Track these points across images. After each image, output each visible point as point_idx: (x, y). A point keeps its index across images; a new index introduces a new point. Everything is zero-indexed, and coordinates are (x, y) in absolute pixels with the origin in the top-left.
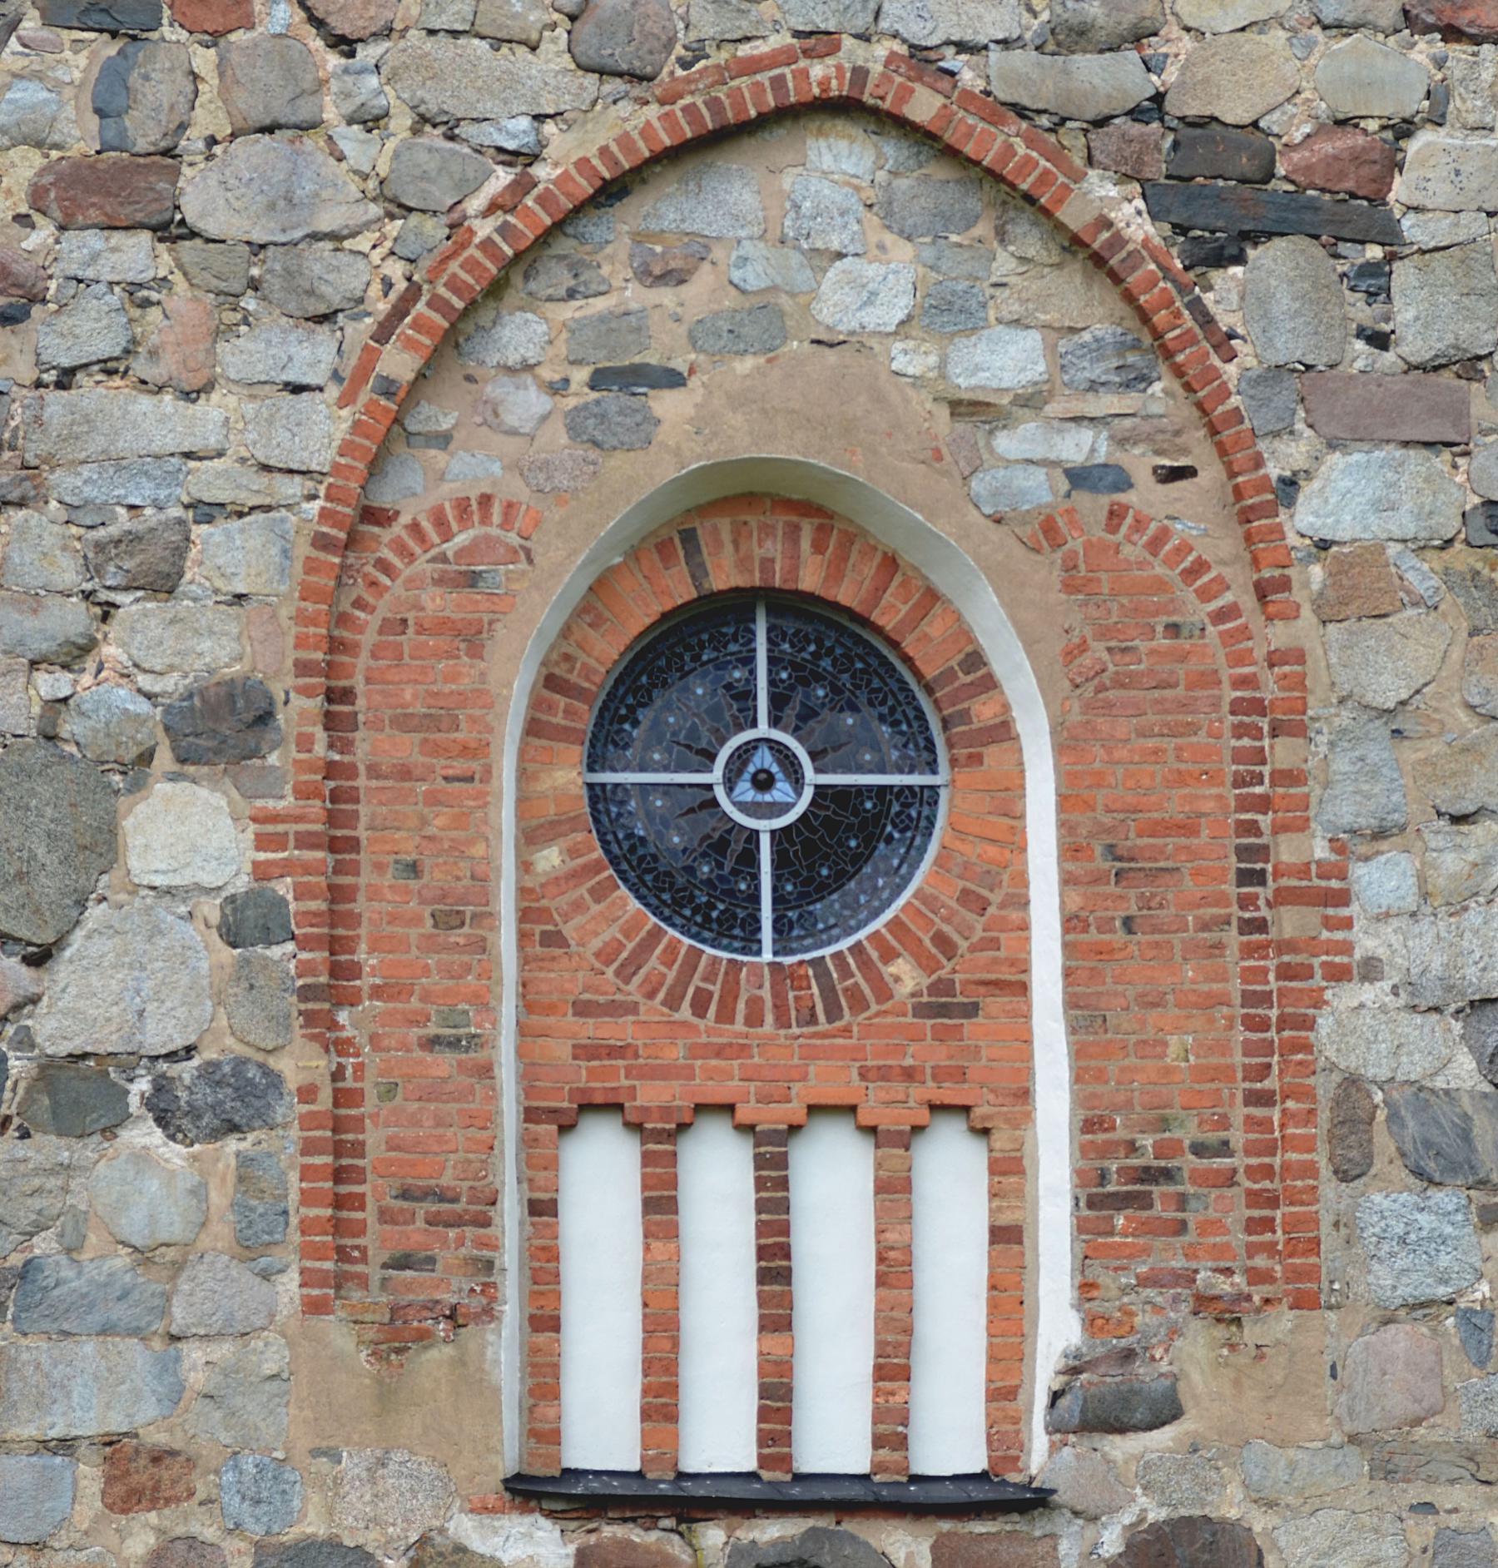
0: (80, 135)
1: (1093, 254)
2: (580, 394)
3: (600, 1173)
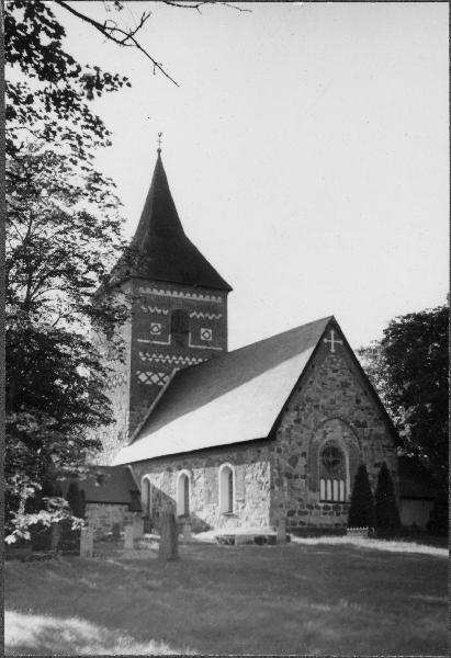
3: (323, 482)
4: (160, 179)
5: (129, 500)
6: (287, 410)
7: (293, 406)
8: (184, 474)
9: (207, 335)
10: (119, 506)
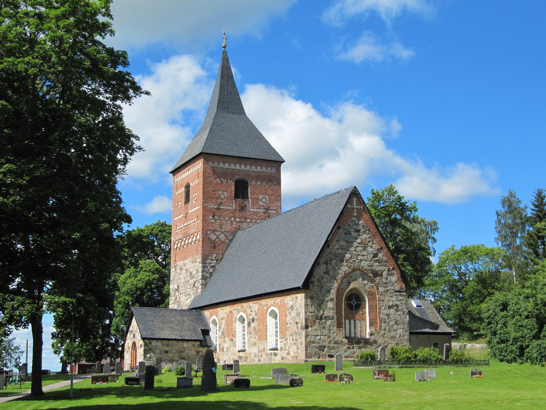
0: (325, 270)
1: (370, 277)
3: (347, 321)
4: (225, 53)
5: (201, 337)
6: (318, 264)
7: (322, 261)
8: (241, 316)
9: (264, 200)
10: (193, 342)
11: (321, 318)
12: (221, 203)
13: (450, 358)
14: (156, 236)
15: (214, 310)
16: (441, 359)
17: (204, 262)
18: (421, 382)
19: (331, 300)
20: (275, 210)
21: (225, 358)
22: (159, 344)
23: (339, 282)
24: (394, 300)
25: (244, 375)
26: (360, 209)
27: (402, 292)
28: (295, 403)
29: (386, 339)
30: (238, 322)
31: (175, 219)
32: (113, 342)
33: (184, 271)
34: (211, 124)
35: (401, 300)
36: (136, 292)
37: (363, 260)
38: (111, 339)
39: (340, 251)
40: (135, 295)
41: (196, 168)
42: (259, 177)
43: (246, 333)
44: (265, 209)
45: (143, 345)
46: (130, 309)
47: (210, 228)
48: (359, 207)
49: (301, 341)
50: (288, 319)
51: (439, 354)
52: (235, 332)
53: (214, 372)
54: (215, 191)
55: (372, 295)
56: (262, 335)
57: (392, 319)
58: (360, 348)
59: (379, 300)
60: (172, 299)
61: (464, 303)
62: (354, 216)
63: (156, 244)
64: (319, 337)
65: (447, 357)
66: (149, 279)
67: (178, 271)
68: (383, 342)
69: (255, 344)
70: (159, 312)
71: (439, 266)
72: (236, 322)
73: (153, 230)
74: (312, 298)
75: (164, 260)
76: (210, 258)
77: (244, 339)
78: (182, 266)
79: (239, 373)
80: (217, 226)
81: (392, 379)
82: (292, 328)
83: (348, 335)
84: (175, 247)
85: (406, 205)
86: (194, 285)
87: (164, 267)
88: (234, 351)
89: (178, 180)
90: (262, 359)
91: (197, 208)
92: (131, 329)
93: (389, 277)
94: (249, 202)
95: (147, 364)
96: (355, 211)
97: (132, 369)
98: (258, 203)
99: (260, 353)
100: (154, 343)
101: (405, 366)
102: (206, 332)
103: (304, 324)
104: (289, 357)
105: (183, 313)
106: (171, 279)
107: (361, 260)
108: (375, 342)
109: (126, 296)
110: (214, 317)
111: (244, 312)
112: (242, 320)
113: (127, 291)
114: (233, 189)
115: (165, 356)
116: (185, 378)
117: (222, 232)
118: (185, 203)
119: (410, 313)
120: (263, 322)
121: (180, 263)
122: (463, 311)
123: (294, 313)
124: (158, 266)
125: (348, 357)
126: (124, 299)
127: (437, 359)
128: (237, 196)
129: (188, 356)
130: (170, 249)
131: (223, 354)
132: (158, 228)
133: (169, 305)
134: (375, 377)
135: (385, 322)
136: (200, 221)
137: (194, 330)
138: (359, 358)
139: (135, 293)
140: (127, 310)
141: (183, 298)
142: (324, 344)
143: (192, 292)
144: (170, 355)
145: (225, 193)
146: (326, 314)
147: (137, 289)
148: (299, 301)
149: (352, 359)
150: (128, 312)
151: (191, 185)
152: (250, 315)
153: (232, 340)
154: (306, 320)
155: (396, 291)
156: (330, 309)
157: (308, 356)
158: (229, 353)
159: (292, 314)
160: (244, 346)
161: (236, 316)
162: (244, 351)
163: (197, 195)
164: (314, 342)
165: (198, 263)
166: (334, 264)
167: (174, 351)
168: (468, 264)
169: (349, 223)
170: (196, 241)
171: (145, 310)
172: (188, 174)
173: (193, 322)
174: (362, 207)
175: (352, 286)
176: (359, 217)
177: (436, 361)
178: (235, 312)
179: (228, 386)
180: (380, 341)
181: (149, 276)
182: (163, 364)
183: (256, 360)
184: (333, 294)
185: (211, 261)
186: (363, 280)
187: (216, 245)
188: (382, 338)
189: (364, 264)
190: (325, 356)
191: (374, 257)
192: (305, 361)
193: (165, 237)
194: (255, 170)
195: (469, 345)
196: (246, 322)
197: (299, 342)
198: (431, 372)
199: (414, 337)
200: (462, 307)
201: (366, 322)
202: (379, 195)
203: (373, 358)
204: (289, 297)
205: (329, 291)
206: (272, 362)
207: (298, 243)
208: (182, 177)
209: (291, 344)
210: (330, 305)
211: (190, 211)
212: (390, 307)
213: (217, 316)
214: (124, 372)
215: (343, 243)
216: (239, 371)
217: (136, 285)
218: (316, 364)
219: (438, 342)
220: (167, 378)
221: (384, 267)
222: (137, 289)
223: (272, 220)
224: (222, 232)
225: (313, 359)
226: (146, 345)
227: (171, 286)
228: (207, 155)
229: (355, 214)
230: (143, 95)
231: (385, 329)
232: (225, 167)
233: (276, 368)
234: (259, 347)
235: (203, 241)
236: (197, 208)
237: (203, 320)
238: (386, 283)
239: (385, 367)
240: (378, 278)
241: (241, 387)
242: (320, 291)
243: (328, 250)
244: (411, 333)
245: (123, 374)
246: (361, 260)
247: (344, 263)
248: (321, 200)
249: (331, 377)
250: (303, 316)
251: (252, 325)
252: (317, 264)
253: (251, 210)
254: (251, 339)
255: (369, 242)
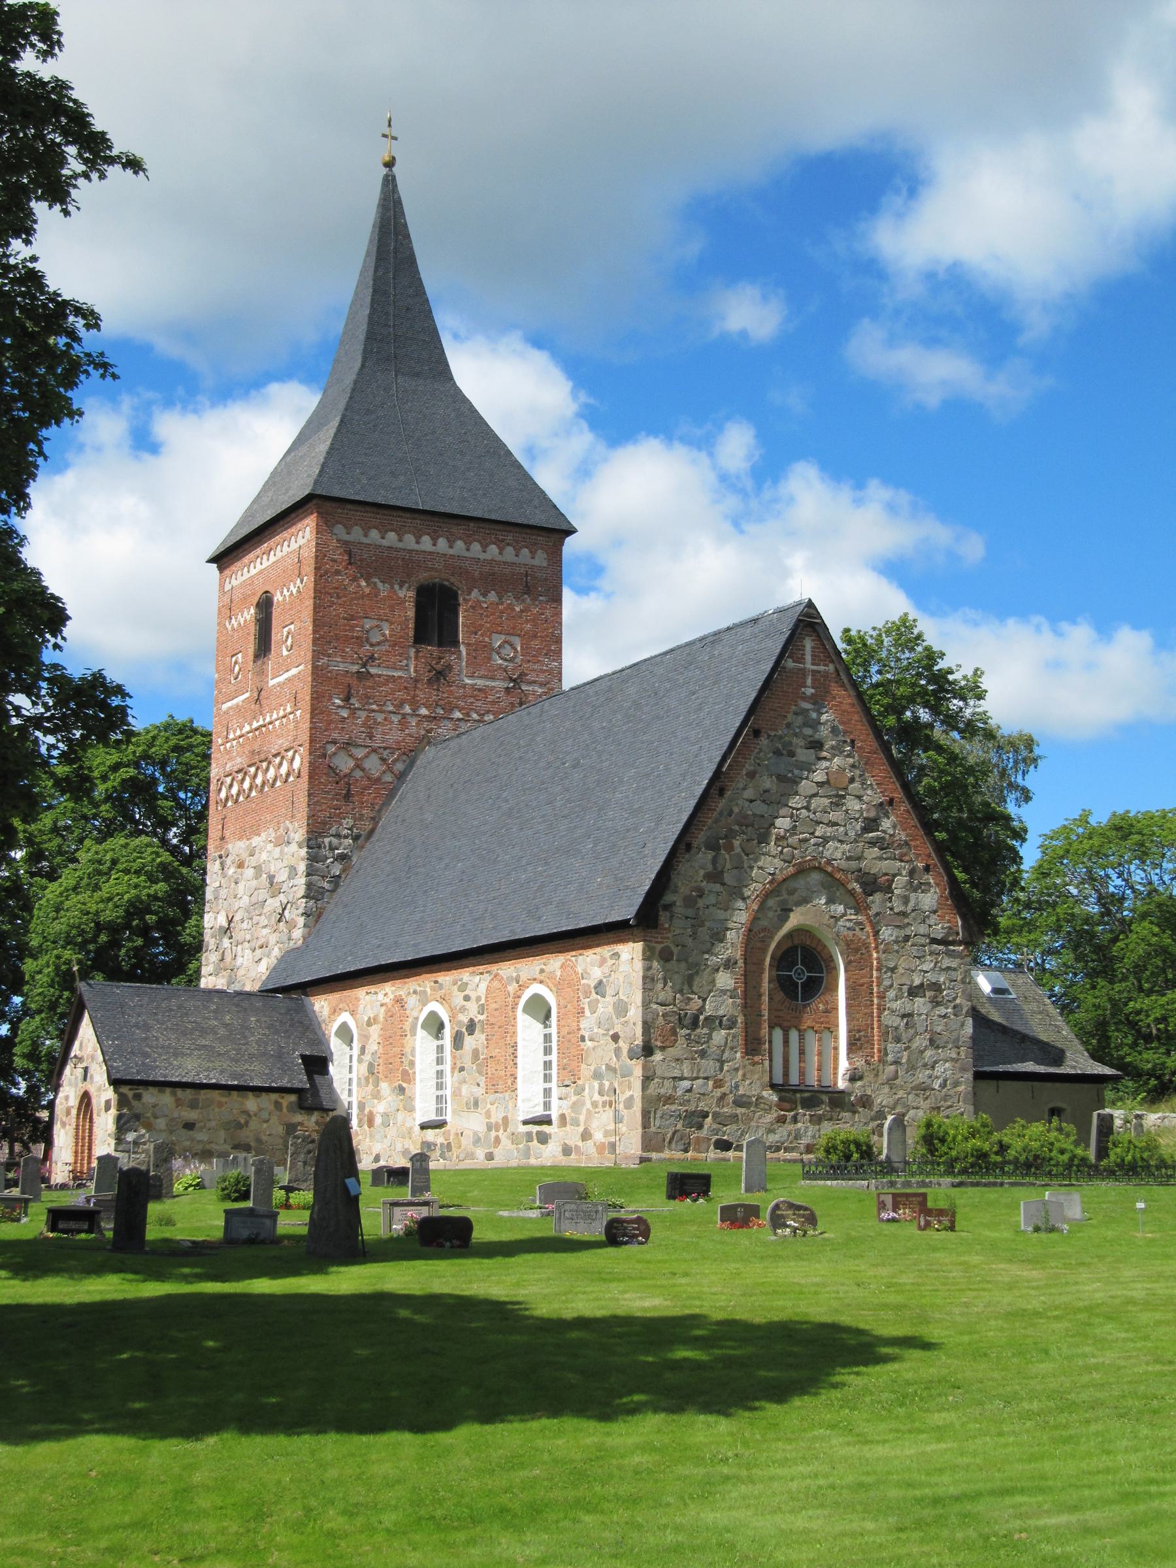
0: (710, 868)
1: (852, 893)
2: (779, 912)
3: (778, 1034)
4: (390, 183)
5: (300, 1080)
6: (689, 847)
7: (700, 838)
10: (274, 1096)
11: (695, 1024)
12: (372, 658)
13: (1112, 1157)
14: (163, 763)
15: (346, 993)
16: (1084, 1160)
17: (313, 842)
18: (1043, 1235)
19: (729, 964)
20: (542, 685)
21: (377, 1148)
22: (167, 1098)
23: (755, 907)
24: (926, 969)
25: (446, 1202)
26: (826, 675)
27: (953, 943)
28: (638, 1304)
29: (901, 1094)
30: (421, 1033)
31: (225, 707)
32: (21, 1093)
33: (249, 873)
34: (342, 405)
35: (949, 968)
36: (96, 936)
37: (833, 838)
38: (16, 1085)
39: (760, 808)
40: (91, 947)
41: (294, 546)
42: (492, 579)
43: (447, 1067)
44: (511, 680)
45: (113, 1103)
46: (73, 990)
47: (335, 735)
48: (822, 668)
49: (628, 1094)
50: (588, 1024)
51: (1077, 1143)
52: (412, 1063)
53: (353, 1193)
54: (352, 618)
55: (857, 953)
56: (502, 1080)
57: (921, 1029)
58: (817, 1120)
59: (879, 969)
60: (209, 961)
61: (1117, 987)
62: (804, 698)
63: (161, 789)
64: (686, 1084)
65: (1102, 1152)
66: (138, 897)
67: (231, 871)
68: (891, 1101)
69: (476, 1104)
70: (168, 999)
71: (1042, 873)
72: (414, 1034)
73: (151, 745)
74: (665, 956)
75: (185, 840)
76: (333, 831)
77: (440, 1086)
78: (244, 855)
79: (427, 1196)
80: (357, 729)
81: (946, 1221)
82: (601, 1053)
83: (778, 1079)
84: (223, 795)
85: (951, 677)
86: (282, 915)
87: (187, 861)
88: (408, 1125)
89: (234, 583)
90: (497, 1152)
91: (294, 671)
92: (75, 1050)
93: (913, 896)
94: (459, 658)
95: (126, 1162)
96: (809, 681)
97: (78, 1179)
98: (490, 659)
99: (493, 1134)
100: (150, 1096)
101: (973, 1179)
102: (317, 1064)
103: (639, 1041)
104: (589, 1147)
105: (245, 1004)
106: (209, 894)
107: (826, 840)
108: (865, 1101)
109: (64, 947)
110: (345, 1017)
111: (443, 1000)
112: (435, 1026)
113: (68, 933)
114: (411, 613)
115: (183, 1138)
116: (251, 1212)
117: (374, 751)
118: (257, 657)
119: (975, 1013)
120: (504, 1033)
121: (237, 847)
122: (1113, 1015)
123: (606, 1006)
124: (166, 857)
125: (778, 1149)
126: (58, 957)
127: (1071, 1159)
128: (421, 637)
129: (259, 1141)
130: (206, 807)
131: (372, 1136)
132: (167, 740)
133: (198, 979)
134: (885, 1216)
135: (898, 1040)
136: (302, 715)
137: (279, 1056)
138: (821, 1154)
139: (94, 940)
140: (66, 994)
141: (245, 958)
142: (702, 1106)
143: (273, 939)
144: (201, 1136)
145: (385, 625)
146: (709, 1009)
147: (99, 928)
148: (624, 967)
149: (794, 1155)
150: (68, 999)
151: (278, 598)
152: (463, 1009)
153: (402, 1090)
154: (647, 1026)
155: (934, 941)
156: (724, 992)
157: (649, 1143)
158: (392, 1131)
159: (600, 1010)
160: (440, 1111)
161: (415, 1014)
162: (439, 1125)
163: (294, 632)
164: (669, 1099)
165: (294, 847)
166: (738, 850)
167: (213, 1124)
168: (1133, 868)
169: (790, 717)
170: (288, 775)
171: (122, 990)
172: (266, 564)
173: (277, 1032)
174: (831, 667)
175: (795, 920)
176: (818, 701)
177: (1069, 1166)
178: (412, 1001)
179: (398, 1239)
180: (882, 1098)
181: (136, 886)
182: (177, 1163)
183: (480, 1154)
184: (733, 943)
185: (335, 841)
186: (830, 901)
187: (354, 789)
188: (886, 1089)
189: (836, 852)
190: (704, 1146)
191: (866, 830)
192: (643, 1160)
193: (189, 767)
194: (482, 556)
195: (1152, 1119)
196: (448, 1032)
197: (623, 1098)
198: (1073, 1202)
199: (989, 1087)
200: (1110, 1000)
201: (836, 1038)
202: (865, 645)
203: (867, 1152)
204: (590, 952)
205: (718, 936)
206: (533, 1161)
207: (621, 781)
208: (246, 576)
209: (595, 1104)
210: (725, 980)
211: (272, 683)
212: (914, 992)
213: (353, 1013)
214: (49, 1188)
215: (768, 783)
216: (428, 1189)
217: (97, 913)
218: (676, 1169)
219: (1063, 1106)
220: (192, 1210)
221: (898, 864)
222: (99, 928)
223: (535, 710)
224: (374, 751)
225: (666, 1154)
226: (122, 1102)
227: (208, 920)
228: (328, 504)
229: (810, 691)
230: (114, 171)
231: (896, 1062)
232: (385, 543)
233: (548, 1180)
234: (488, 1114)
235: (311, 777)
236: (294, 671)
237: (309, 1028)
238: (903, 914)
239: (907, 1184)
240: (878, 897)
241: (441, 1246)
242: (694, 935)
243: (722, 804)
244: (979, 1076)
245: (46, 1195)
246: (826, 840)
247: (772, 847)
248: (699, 645)
249: (740, 1213)
250: (635, 1013)
251: (469, 1042)
252: (683, 847)
253: (468, 681)
254: (465, 1089)
255: (852, 780)
